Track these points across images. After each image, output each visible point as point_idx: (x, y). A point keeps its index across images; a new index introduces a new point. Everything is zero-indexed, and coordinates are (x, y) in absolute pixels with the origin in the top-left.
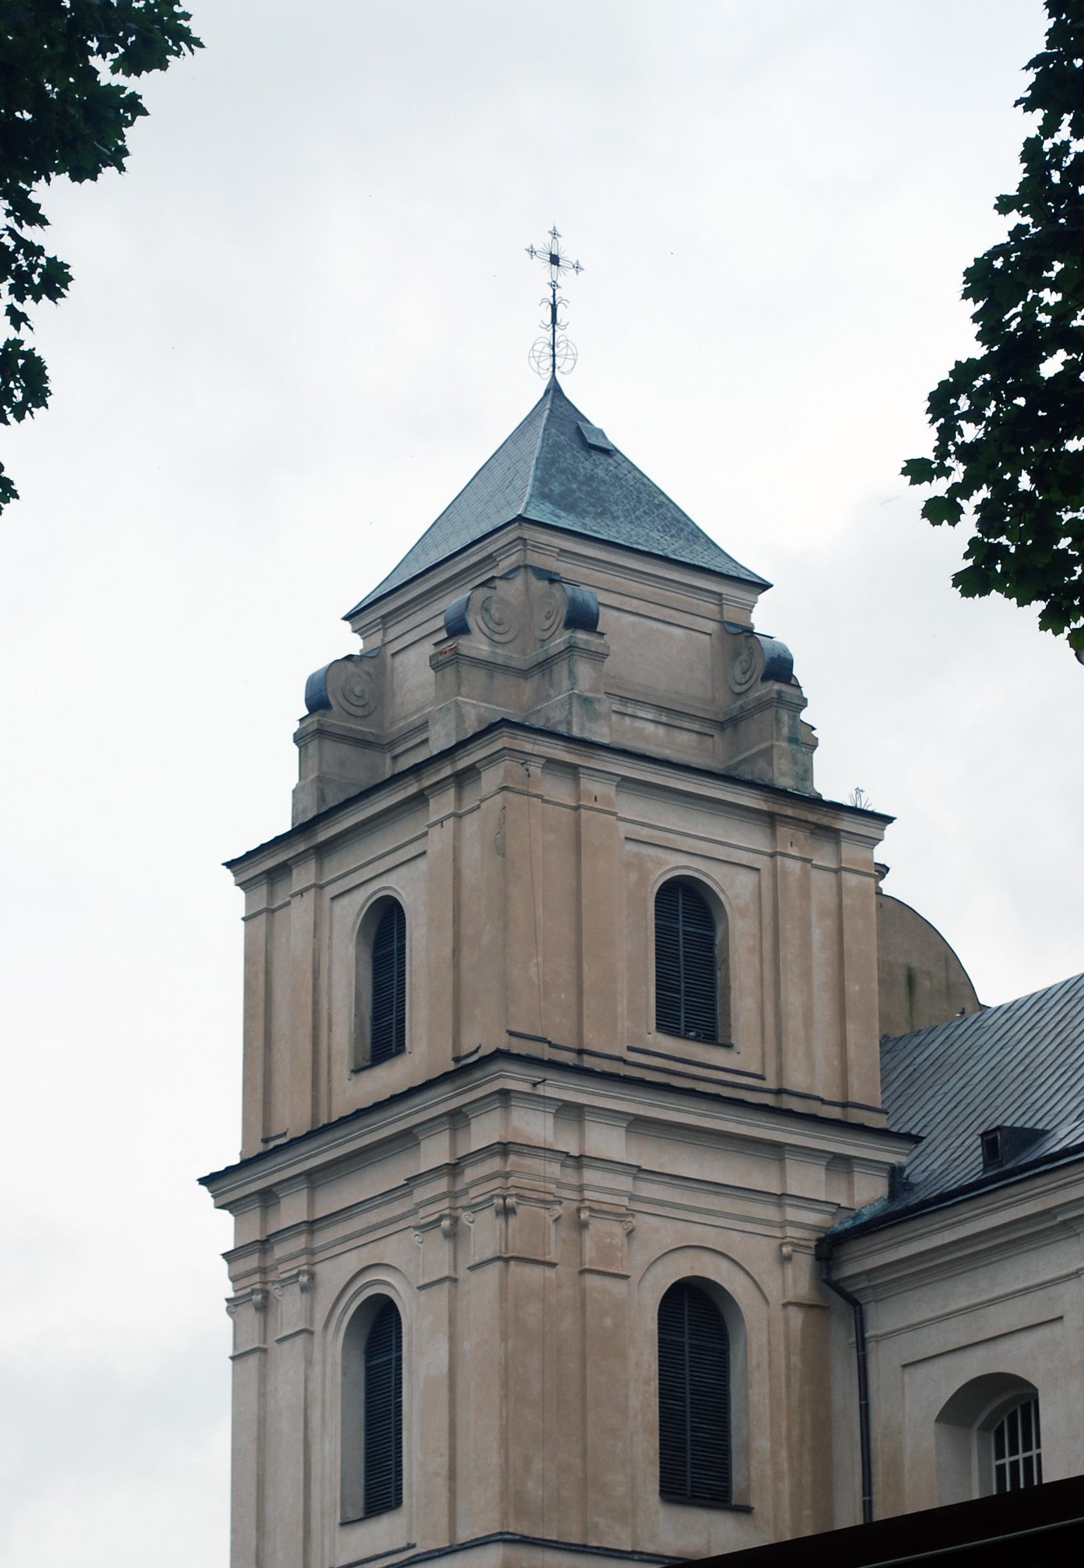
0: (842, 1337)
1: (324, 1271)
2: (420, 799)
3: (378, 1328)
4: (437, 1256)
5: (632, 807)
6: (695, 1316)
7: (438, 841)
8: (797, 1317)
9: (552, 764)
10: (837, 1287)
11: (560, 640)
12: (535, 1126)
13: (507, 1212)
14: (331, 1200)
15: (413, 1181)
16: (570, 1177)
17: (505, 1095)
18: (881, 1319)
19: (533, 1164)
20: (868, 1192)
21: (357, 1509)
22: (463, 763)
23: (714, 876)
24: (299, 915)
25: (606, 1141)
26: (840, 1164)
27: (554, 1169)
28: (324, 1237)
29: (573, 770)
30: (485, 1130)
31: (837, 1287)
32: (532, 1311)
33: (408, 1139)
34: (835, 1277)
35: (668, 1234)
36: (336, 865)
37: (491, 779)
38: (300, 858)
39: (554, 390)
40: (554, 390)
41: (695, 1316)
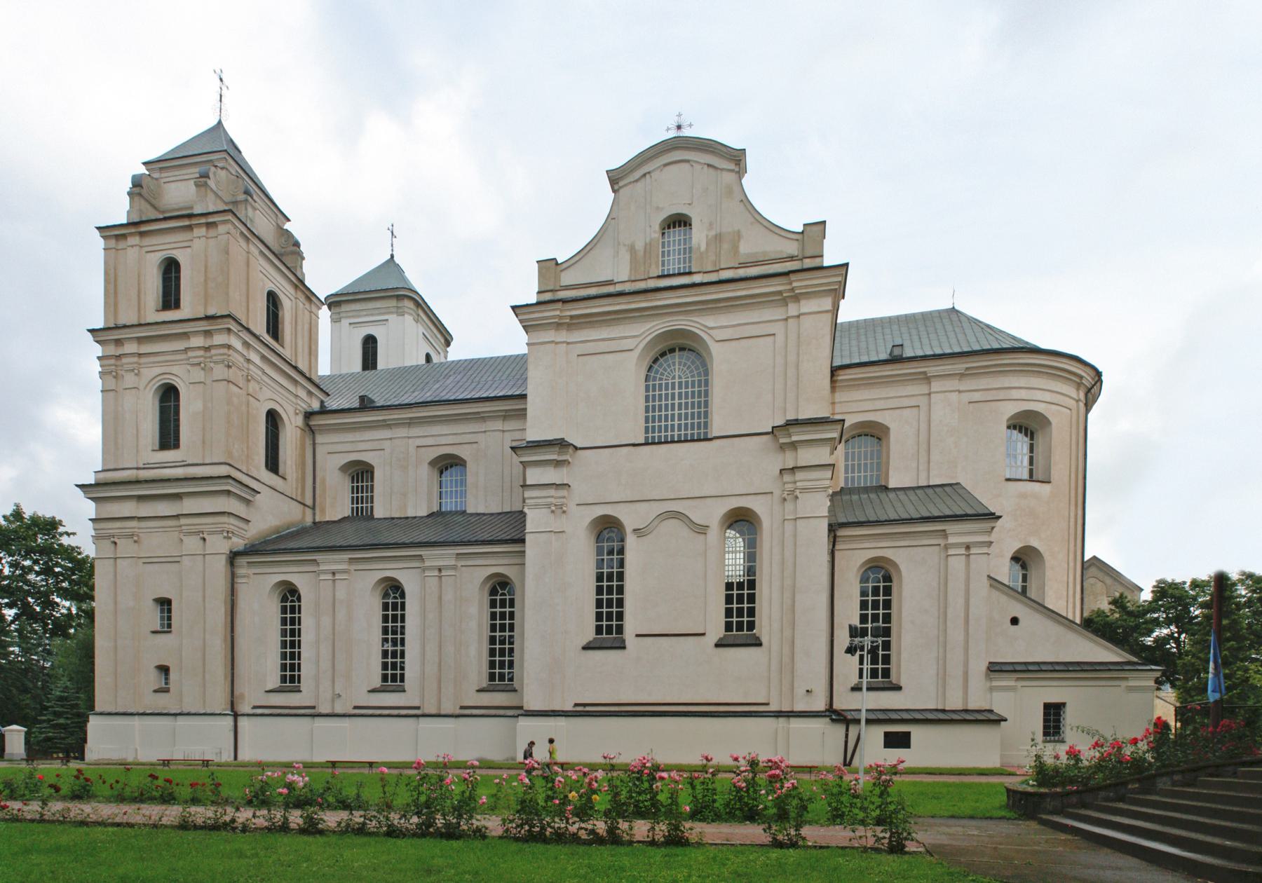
0: (308, 442)
1: (144, 371)
2: (190, 228)
3: (169, 394)
4: (198, 374)
5: (262, 261)
6: (273, 419)
7: (198, 245)
8: (299, 431)
9: (242, 233)
10: (308, 425)
11: (242, 197)
12: (237, 344)
13: (229, 367)
14: (146, 349)
15: (187, 350)
16: (246, 365)
17: (229, 330)
18: (320, 439)
19: (236, 355)
20: (316, 406)
21: (157, 447)
22: (211, 220)
23: (282, 296)
24: (132, 254)
25: (255, 358)
26: (310, 393)
27: (241, 360)
28: (143, 360)
29: (247, 239)
30: (219, 339)
31: (308, 425)
32: (235, 400)
33: (185, 335)
34: (312, 423)
35: (269, 394)
36: (148, 241)
37: (222, 229)
38: (132, 234)
39: (220, 123)
40: (220, 123)
41: (273, 419)
